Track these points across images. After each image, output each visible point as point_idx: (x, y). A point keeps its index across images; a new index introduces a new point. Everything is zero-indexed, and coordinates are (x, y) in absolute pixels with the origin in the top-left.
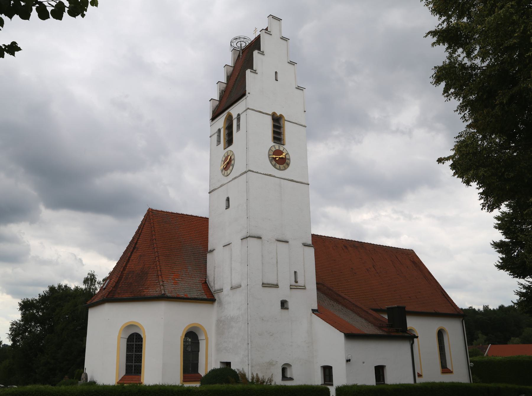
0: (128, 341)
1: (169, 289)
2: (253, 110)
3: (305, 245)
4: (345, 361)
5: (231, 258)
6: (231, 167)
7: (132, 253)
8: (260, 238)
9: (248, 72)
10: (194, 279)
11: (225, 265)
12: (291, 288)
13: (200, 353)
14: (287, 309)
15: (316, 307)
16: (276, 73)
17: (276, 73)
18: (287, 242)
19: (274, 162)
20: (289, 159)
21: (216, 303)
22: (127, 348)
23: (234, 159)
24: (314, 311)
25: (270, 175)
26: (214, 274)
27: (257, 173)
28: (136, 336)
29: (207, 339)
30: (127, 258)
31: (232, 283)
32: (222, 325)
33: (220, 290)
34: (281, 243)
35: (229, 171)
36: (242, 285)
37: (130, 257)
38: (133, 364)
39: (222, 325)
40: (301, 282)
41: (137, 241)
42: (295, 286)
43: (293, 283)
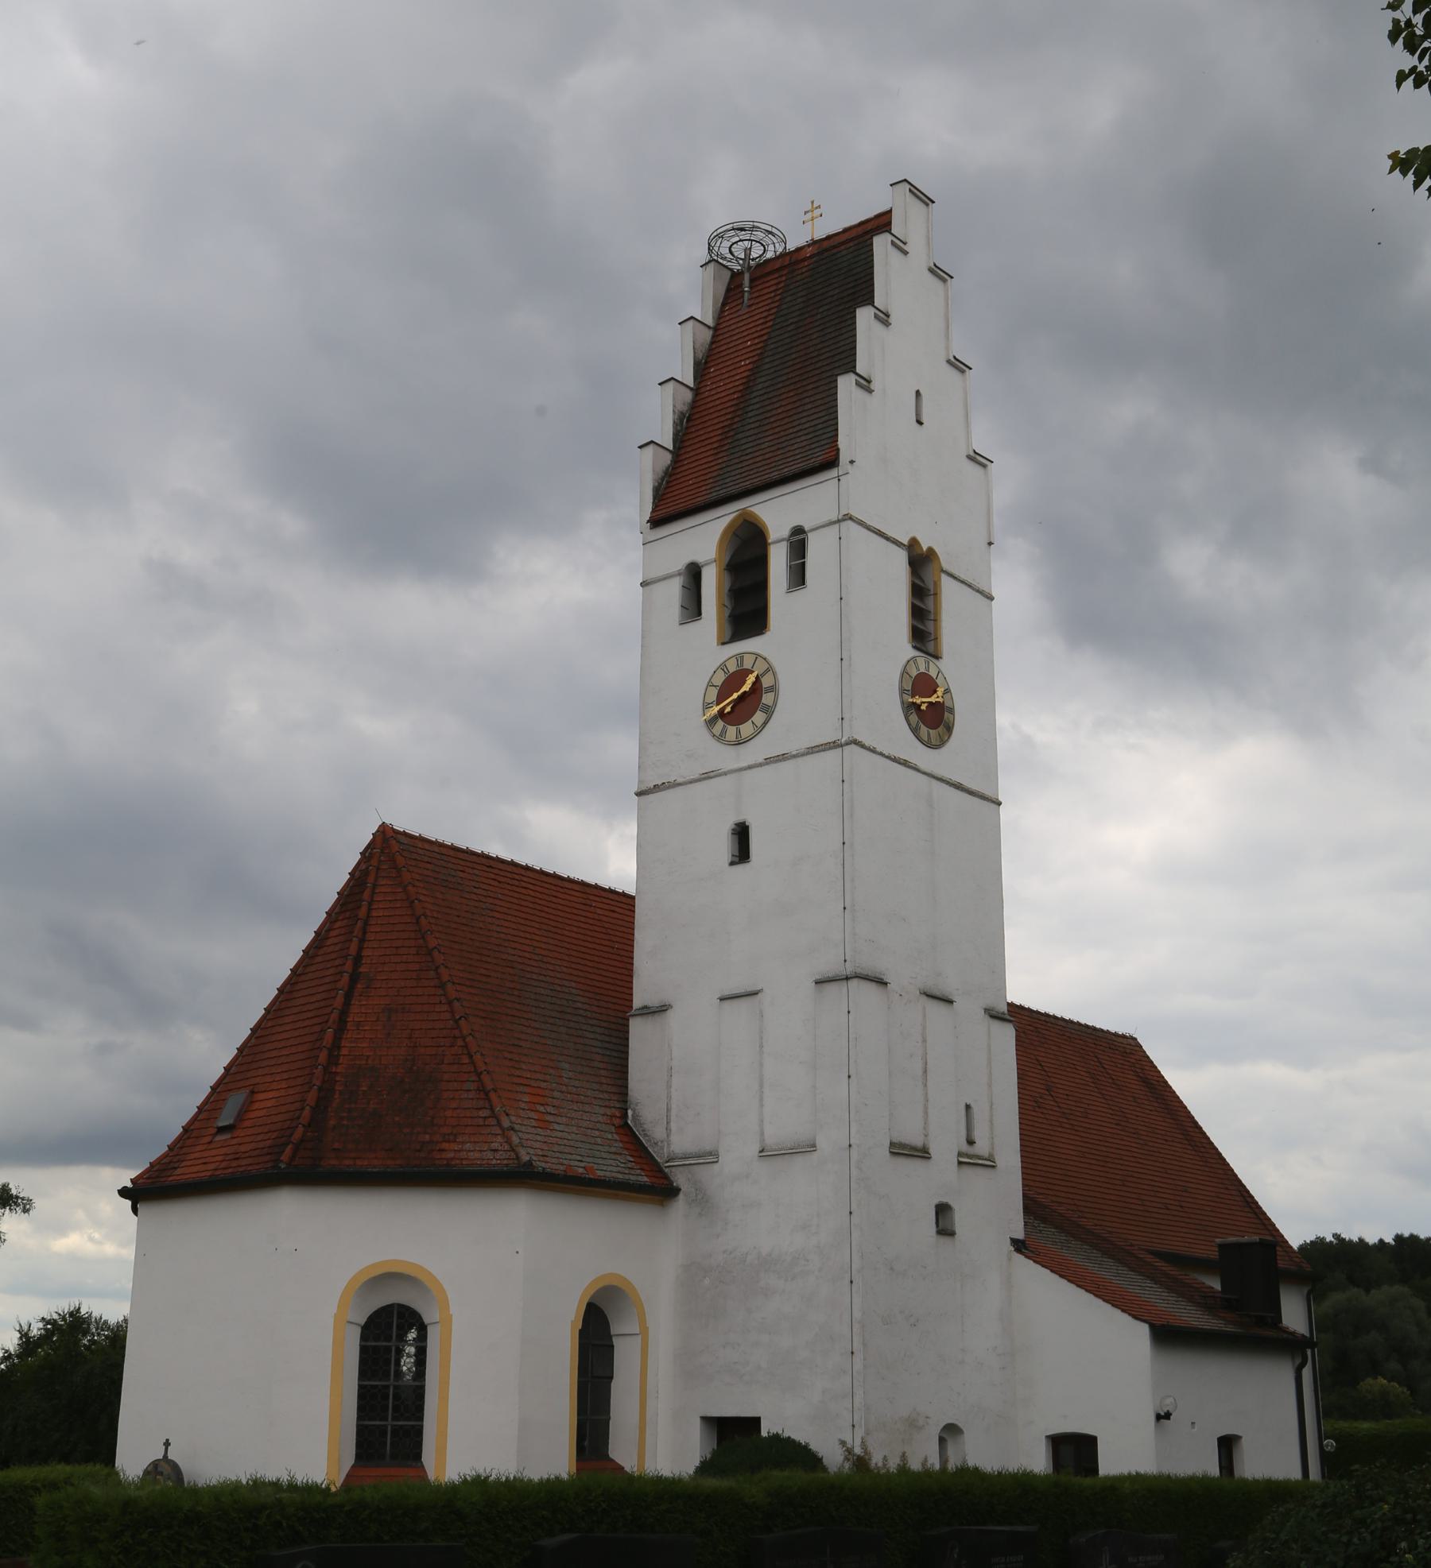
0: (363, 1338)
1: (531, 1148)
2: (861, 523)
3: (993, 1017)
4: (1153, 1418)
5: (761, 1046)
6: (759, 717)
7: (348, 996)
8: (882, 983)
9: (846, 385)
10: (587, 1108)
11: (694, 1066)
12: (960, 1163)
13: (616, 1386)
14: (952, 1234)
15: (1020, 1235)
16: (918, 393)
17: (918, 393)
18: (951, 1002)
19: (914, 718)
20: (951, 711)
21: (680, 1205)
22: (363, 1362)
23: (773, 689)
24: (1019, 1246)
25: (905, 763)
26: (669, 1097)
27: (873, 751)
28: (401, 1315)
29: (644, 1332)
30: (335, 1015)
31: (762, 1134)
32: (708, 1287)
33: (710, 1154)
34: (741, 991)
35: (746, 729)
36: (821, 1143)
37: (344, 1013)
38: (390, 1423)
39: (708, 1287)
40: (982, 1147)
41: (360, 949)
42: (971, 1160)
43: (965, 1148)
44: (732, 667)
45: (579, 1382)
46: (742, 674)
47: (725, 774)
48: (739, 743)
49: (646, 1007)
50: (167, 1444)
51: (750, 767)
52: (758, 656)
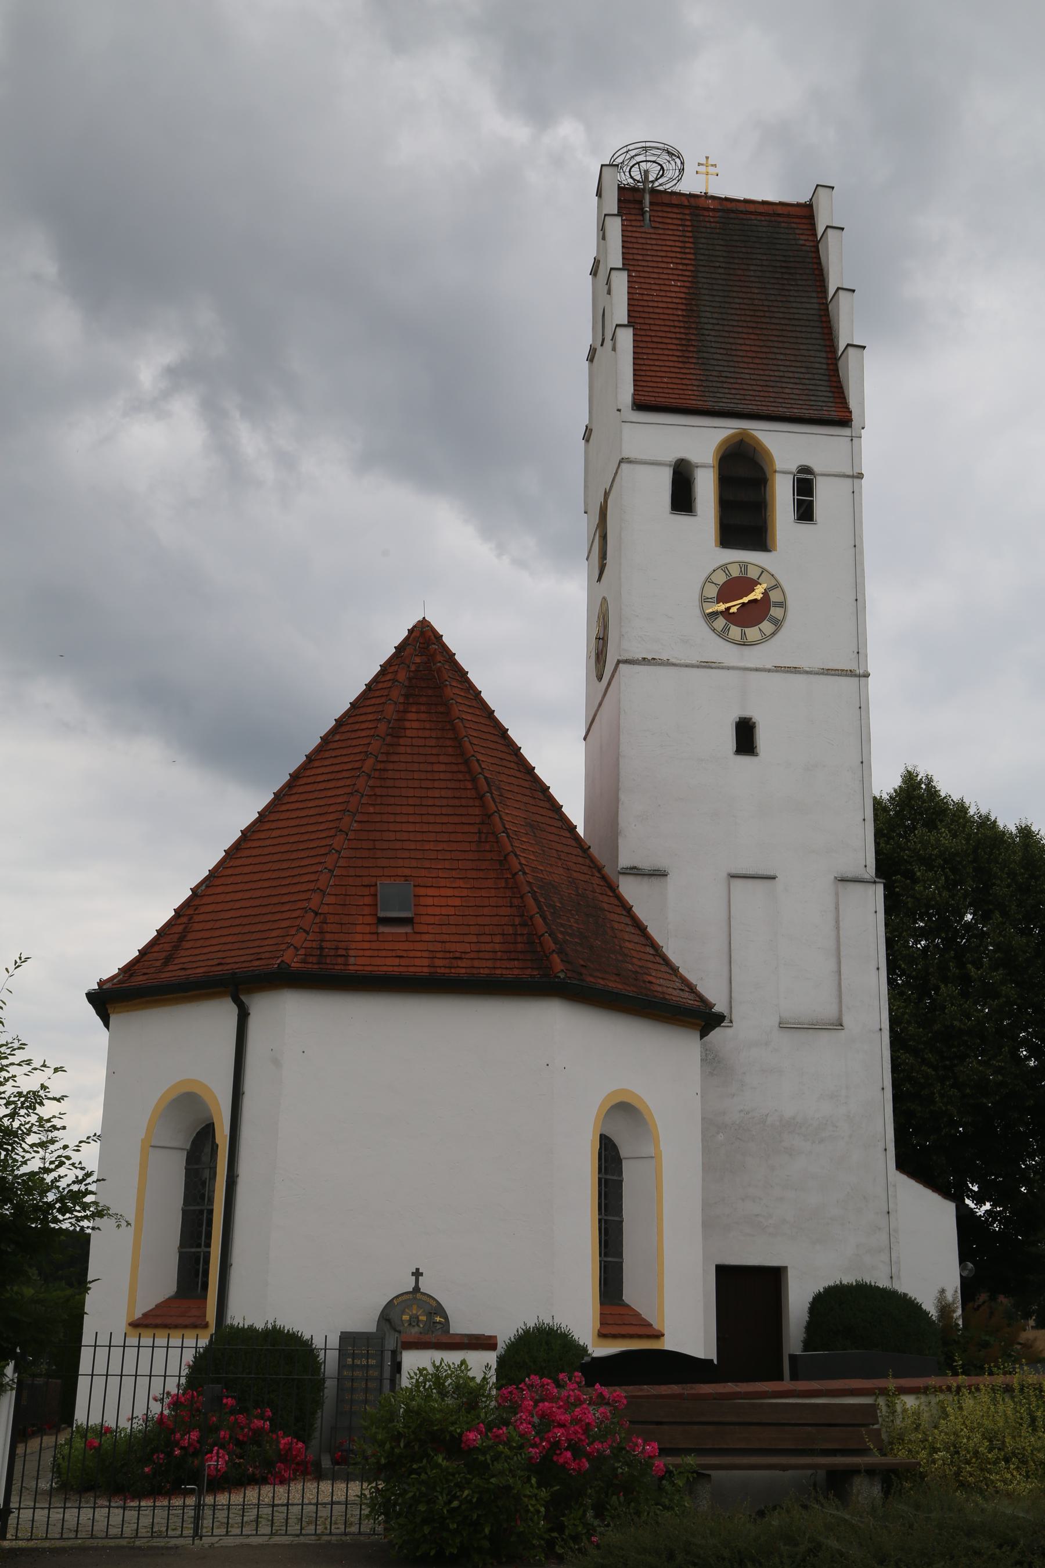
6: (766, 626)
23: (782, 605)
34: (751, 872)
35: (752, 633)
44: (735, 572)
45: (185, 1212)
46: (750, 585)
47: (728, 668)
48: (744, 643)
49: (635, 868)
50: (417, 1274)
51: (757, 670)
52: (763, 570)
